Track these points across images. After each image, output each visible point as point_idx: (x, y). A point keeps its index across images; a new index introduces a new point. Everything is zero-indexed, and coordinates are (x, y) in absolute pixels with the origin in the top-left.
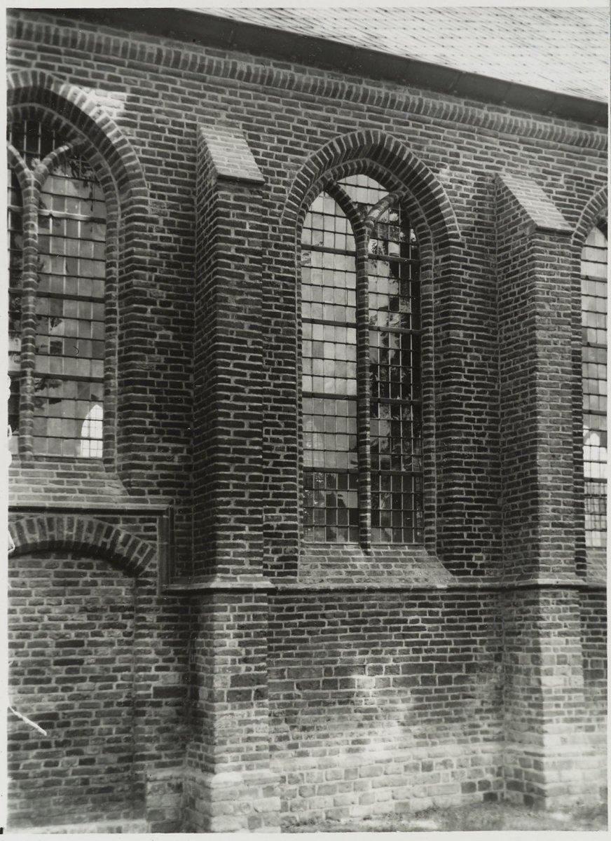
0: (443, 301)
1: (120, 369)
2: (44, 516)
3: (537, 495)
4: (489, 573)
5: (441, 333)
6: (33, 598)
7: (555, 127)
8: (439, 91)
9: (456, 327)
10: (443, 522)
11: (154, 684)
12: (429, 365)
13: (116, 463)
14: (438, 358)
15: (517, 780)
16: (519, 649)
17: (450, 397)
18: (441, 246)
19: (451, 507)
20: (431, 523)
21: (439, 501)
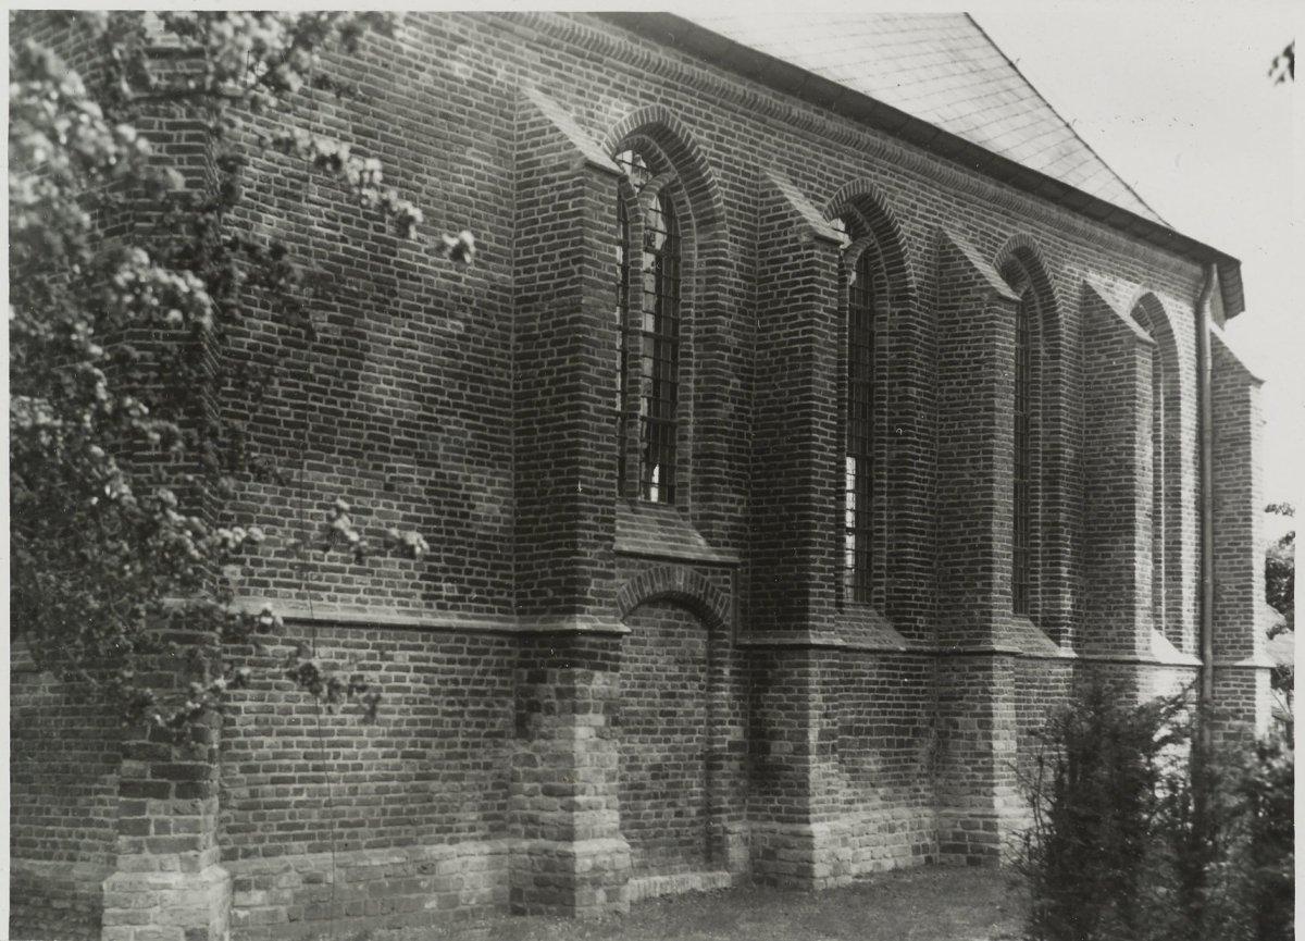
0: (899, 356)
1: (696, 414)
2: (664, 565)
3: (991, 562)
4: (930, 636)
5: (897, 388)
6: (648, 648)
7: (749, 91)
8: (967, 165)
9: (913, 385)
10: (894, 583)
11: (729, 738)
12: (882, 420)
13: (691, 511)
14: (891, 414)
15: (709, 874)
16: (960, 714)
17: (906, 455)
18: (898, 298)
19: (904, 568)
20: (880, 584)
21: (889, 561)
